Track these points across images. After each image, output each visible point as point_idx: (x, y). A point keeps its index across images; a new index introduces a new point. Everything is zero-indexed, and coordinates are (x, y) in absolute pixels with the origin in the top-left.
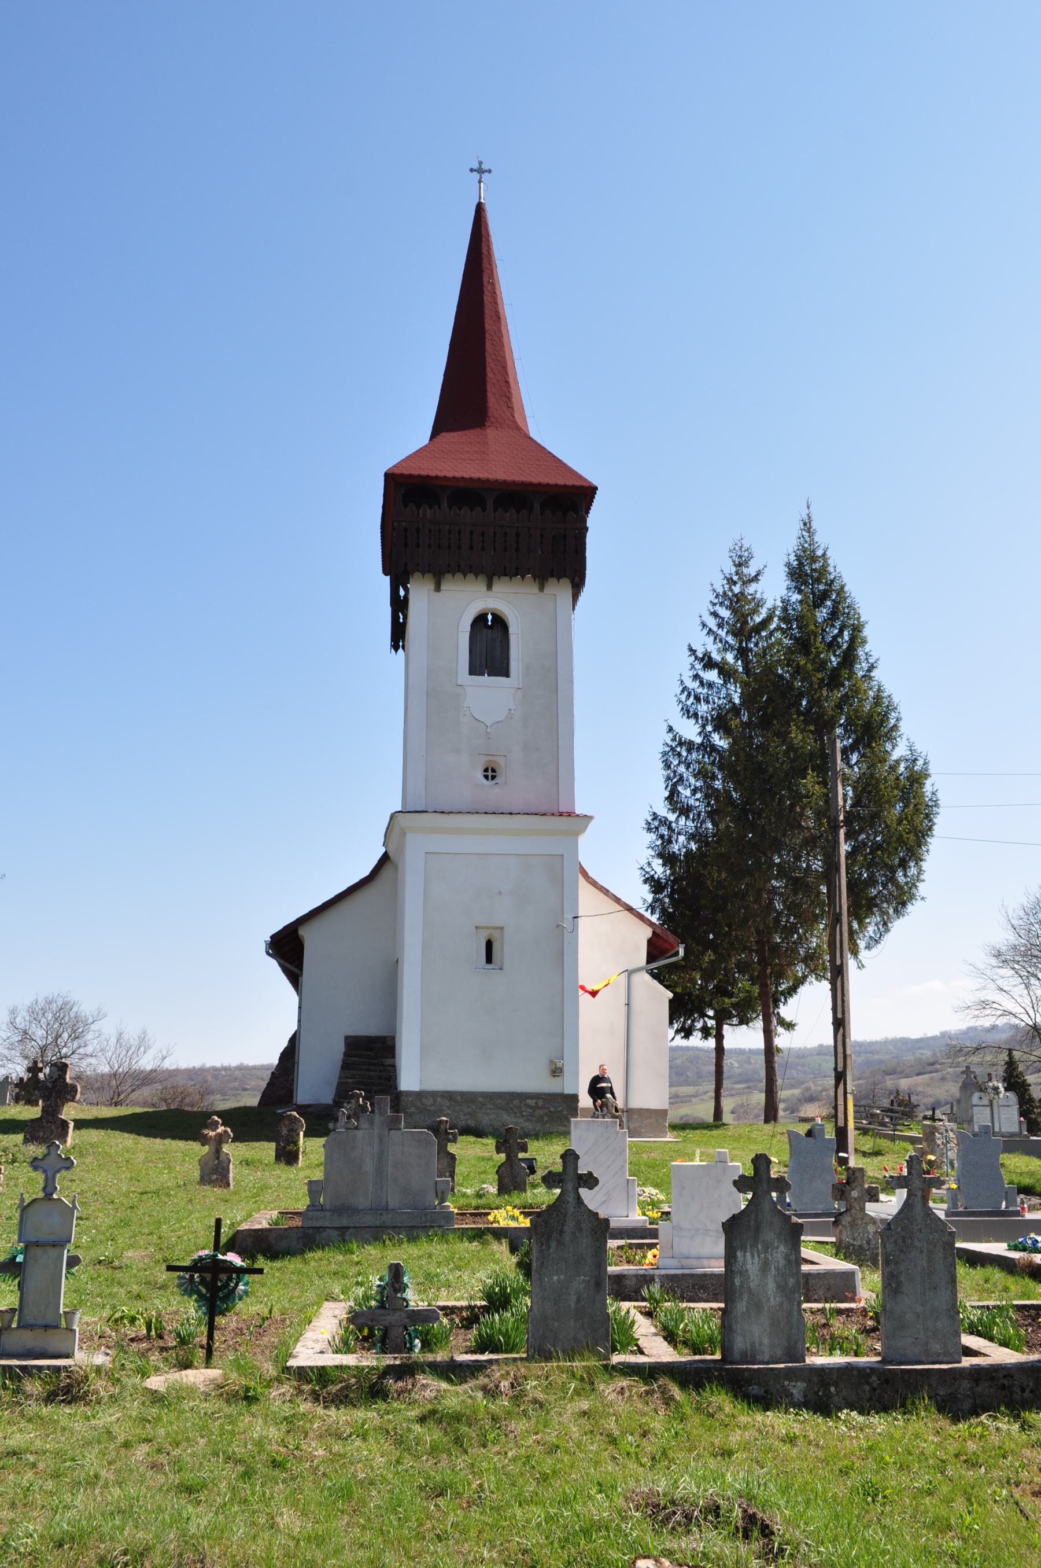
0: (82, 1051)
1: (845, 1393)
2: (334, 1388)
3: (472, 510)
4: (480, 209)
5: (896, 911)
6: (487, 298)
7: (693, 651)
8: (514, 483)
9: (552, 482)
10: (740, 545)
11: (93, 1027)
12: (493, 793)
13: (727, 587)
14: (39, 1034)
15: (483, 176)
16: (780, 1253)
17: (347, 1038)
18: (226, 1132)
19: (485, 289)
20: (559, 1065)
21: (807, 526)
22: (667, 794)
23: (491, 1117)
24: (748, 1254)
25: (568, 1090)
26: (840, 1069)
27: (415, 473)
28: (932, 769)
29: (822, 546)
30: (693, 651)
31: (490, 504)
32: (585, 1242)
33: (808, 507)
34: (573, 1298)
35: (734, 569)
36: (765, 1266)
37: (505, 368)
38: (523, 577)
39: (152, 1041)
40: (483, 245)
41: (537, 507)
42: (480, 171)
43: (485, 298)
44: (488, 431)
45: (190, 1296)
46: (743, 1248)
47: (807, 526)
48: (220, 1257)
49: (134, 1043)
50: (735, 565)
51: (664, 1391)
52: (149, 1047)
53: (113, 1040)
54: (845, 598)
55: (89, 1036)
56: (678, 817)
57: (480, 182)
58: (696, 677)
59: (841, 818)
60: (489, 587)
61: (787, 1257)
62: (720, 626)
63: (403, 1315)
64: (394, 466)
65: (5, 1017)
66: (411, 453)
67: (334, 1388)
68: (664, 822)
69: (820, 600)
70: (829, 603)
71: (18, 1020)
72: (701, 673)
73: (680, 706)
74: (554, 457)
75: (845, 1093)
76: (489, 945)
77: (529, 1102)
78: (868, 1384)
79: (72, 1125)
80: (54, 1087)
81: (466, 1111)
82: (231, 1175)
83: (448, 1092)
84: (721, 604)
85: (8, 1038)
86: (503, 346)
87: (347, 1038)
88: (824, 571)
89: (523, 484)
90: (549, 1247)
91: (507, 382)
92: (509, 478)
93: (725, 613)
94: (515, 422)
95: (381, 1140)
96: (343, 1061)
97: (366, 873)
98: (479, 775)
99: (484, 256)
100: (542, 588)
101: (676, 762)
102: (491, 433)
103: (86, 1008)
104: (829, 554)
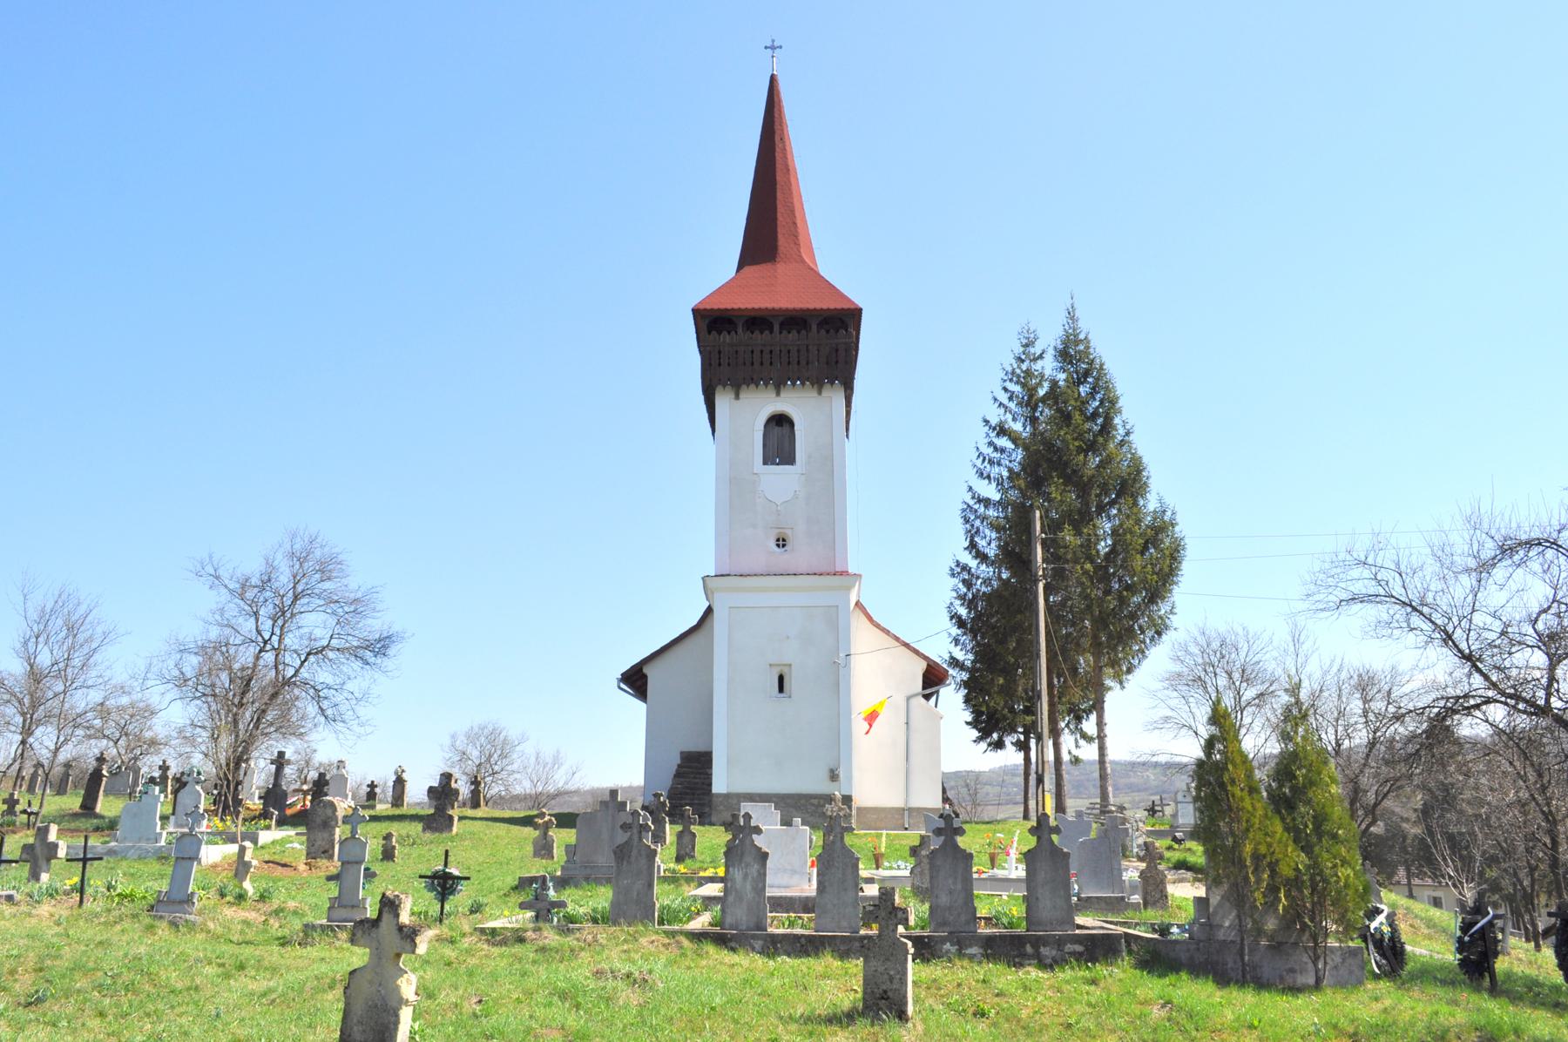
0: (509, 768)
2: (498, 938)
3: (762, 333)
4: (773, 79)
5: (1152, 639)
6: (778, 155)
8: (794, 310)
9: (825, 307)
11: (518, 748)
12: (782, 559)
13: (1015, 366)
14: (474, 753)
17: (682, 753)
18: (550, 820)
21: (1072, 316)
22: (967, 544)
27: (716, 307)
28: (1179, 518)
30: (986, 422)
31: (776, 328)
32: (643, 861)
35: (1022, 349)
36: (746, 876)
37: (793, 212)
40: (776, 110)
41: (814, 327)
42: (773, 48)
46: (733, 866)
47: (1072, 316)
48: (447, 870)
49: (550, 760)
50: (1023, 346)
51: (678, 942)
53: (533, 759)
54: (1105, 374)
55: (515, 756)
58: (991, 444)
59: (1041, 573)
60: (778, 394)
62: (1010, 399)
65: (447, 741)
66: (723, 282)
67: (498, 938)
68: (965, 568)
69: (1082, 378)
70: (1090, 380)
72: (996, 441)
73: (975, 470)
75: (1043, 791)
76: (781, 679)
77: (813, 801)
79: (456, 819)
80: (443, 791)
82: (555, 851)
83: (749, 794)
84: (1011, 380)
87: (682, 753)
88: (1086, 352)
91: (795, 223)
92: (790, 306)
93: (1017, 389)
94: (801, 256)
96: (677, 771)
97: (695, 623)
98: (772, 544)
100: (820, 393)
101: (972, 517)
103: (512, 733)
104: (1090, 337)
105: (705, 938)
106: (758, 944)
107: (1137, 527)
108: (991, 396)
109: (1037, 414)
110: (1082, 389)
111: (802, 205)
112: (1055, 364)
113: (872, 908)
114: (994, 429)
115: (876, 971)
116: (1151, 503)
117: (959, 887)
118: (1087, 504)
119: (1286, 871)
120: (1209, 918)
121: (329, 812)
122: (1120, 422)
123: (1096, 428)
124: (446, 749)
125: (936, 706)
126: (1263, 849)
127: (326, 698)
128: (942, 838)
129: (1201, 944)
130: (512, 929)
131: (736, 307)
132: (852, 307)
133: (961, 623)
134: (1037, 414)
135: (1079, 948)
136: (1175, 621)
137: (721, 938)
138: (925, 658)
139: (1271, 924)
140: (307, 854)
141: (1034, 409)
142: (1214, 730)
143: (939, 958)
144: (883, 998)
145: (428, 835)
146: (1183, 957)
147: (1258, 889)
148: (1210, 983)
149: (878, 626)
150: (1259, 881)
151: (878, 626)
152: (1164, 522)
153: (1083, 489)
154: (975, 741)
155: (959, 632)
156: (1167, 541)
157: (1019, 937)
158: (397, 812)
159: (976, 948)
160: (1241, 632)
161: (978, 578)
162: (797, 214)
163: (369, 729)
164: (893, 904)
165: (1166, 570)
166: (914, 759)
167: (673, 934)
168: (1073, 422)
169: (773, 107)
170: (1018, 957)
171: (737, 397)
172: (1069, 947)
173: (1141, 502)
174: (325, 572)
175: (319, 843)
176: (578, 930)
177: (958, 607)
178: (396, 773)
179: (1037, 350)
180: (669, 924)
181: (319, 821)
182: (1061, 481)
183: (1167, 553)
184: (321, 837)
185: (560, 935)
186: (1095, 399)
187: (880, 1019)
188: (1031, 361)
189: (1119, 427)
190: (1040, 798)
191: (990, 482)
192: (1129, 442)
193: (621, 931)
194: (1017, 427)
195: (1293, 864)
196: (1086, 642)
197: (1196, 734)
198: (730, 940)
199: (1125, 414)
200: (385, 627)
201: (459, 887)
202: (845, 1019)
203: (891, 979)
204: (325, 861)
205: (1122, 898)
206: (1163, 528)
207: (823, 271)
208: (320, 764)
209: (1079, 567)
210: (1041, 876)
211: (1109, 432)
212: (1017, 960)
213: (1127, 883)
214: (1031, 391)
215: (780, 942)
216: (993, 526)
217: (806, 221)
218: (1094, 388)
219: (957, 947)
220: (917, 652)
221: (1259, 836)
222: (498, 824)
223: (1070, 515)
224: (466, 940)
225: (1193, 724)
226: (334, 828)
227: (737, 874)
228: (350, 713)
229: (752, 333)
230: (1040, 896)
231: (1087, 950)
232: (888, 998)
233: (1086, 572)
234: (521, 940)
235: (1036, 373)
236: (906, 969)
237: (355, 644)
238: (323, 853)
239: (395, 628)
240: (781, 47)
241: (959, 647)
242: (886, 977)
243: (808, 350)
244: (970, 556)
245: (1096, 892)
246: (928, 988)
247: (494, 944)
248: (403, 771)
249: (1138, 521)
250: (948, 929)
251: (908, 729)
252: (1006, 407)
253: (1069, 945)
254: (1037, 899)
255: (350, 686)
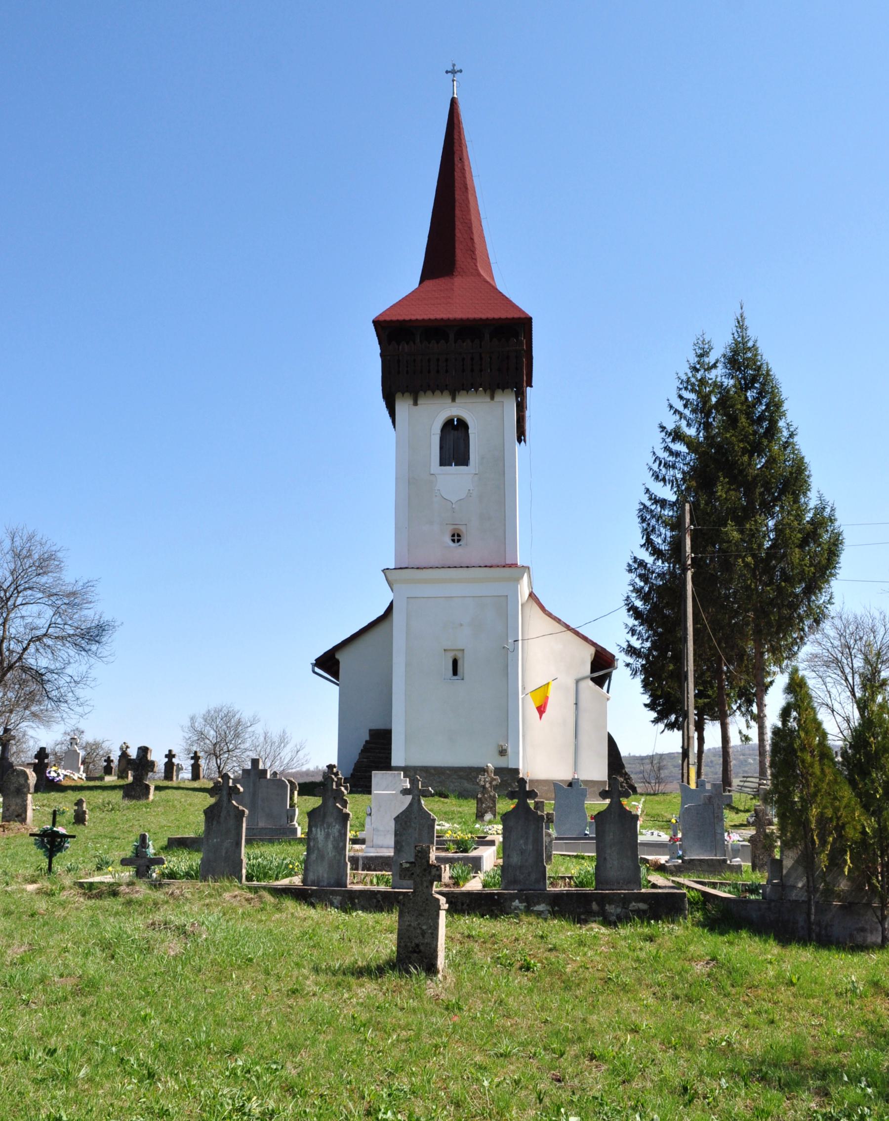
0: (242, 746)
1: (362, 903)
2: (94, 892)
3: (438, 343)
4: (453, 103)
5: (810, 627)
6: (457, 174)
7: (663, 428)
8: (468, 320)
9: (496, 316)
10: (701, 339)
11: (250, 729)
12: (457, 553)
13: (690, 375)
15: (456, 75)
16: (335, 830)
17: (370, 731)
19: (456, 167)
20: (504, 747)
21: (741, 325)
22: (643, 541)
23: (456, 784)
24: (319, 830)
25: (512, 766)
26: (686, 747)
27: (394, 318)
28: (837, 514)
29: (753, 339)
30: (663, 428)
31: (452, 337)
32: (232, 822)
33: (742, 308)
34: (224, 851)
35: (696, 359)
36: (327, 836)
37: (470, 228)
38: (476, 390)
39: (289, 738)
41: (487, 337)
42: (453, 72)
43: (456, 173)
44: (455, 279)
45: (41, 849)
47: (741, 325)
48: (55, 829)
49: (276, 739)
50: (699, 356)
51: (260, 897)
52: (287, 743)
53: (262, 739)
56: (655, 560)
57: (453, 81)
60: (454, 400)
61: (340, 831)
62: (685, 406)
63: (146, 860)
64: (380, 315)
65: (187, 723)
67: (94, 892)
68: (642, 564)
71: (196, 724)
72: (672, 445)
73: (651, 473)
74: (503, 296)
75: (688, 764)
76: (455, 663)
78: (376, 898)
81: (438, 780)
83: (425, 767)
84: (686, 389)
85: (190, 738)
86: (469, 211)
87: (370, 731)
88: (754, 360)
89: (475, 320)
90: (212, 825)
91: (472, 239)
93: (692, 396)
94: (477, 270)
95: (254, 784)
96: (364, 746)
97: (381, 612)
98: (448, 539)
99: (455, 141)
102: (458, 281)
103: (246, 715)
104: (758, 344)
105: (286, 894)
106: (337, 900)
107: (796, 523)
108: (667, 403)
109: (711, 420)
110: (749, 394)
111: (481, 222)
112: (724, 371)
113: (408, 865)
114: (670, 434)
115: (410, 925)
116: (812, 500)
117: (530, 847)
118: (751, 502)
119: (851, 833)
120: (781, 880)
121: (22, 781)
122: (785, 425)
123: (762, 431)
124: (186, 730)
125: (608, 692)
126: (829, 813)
127: (49, 681)
128: (516, 801)
129: (773, 904)
130: (108, 883)
131: (413, 318)
132: (522, 316)
133: (636, 613)
134: (711, 420)
135: (643, 906)
136: (832, 610)
137: (300, 895)
138: (594, 644)
139: (843, 885)
140: (3, 818)
141: (708, 415)
142: (791, 698)
143: (508, 914)
144: (415, 952)
145: (126, 802)
146: (754, 916)
147: (823, 851)
148: (771, 941)
149: (550, 615)
150: (824, 842)
151: (550, 615)
152: (824, 518)
153: (749, 487)
154: (653, 722)
155: (636, 623)
156: (826, 537)
157: (586, 895)
158: (196, 784)
159: (543, 905)
160: (877, 614)
161: (653, 572)
162: (475, 231)
163: (87, 709)
164: (428, 861)
165: (824, 562)
166: (583, 738)
167: (255, 890)
168: (739, 424)
169: (454, 128)
170: (583, 914)
171: (416, 403)
172: (634, 905)
173: (802, 500)
174: (44, 565)
175: (13, 807)
176: (168, 884)
177: (633, 599)
178: (121, 749)
179: (711, 359)
180: (258, 881)
181: (12, 788)
182: (727, 480)
183: (826, 547)
184: (14, 802)
185: (150, 889)
186: (761, 404)
187: (408, 972)
188: (705, 370)
189: (784, 429)
190: (685, 771)
191: (665, 484)
192: (794, 444)
193: (206, 887)
194: (691, 432)
195: (859, 827)
196: (749, 630)
197: (833, 711)
198: (311, 896)
199: (790, 416)
200: (97, 617)
201: (66, 845)
202: (375, 972)
203: (423, 934)
204: (18, 824)
205: (725, 861)
206: (822, 524)
207: (501, 287)
208: (87, 743)
209: (740, 560)
210: (610, 837)
211: (774, 434)
212: (583, 917)
213: (730, 846)
214: (705, 399)
215: (358, 898)
216: (665, 524)
217: (484, 237)
218: (760, 393)
219: (525, 904)
220: (585, 639)
221: (827, 801)
222: (197, 793)
223: (734, 512)
224: (65, 893)
225: (830, 703)
226: (26, 795)
227: (320, 834)
228: (71, 694)
229: (429, 343)
230: (608, 857)
231: (650, 908)
232: (420, 952)
233: (747, 565)
234: (115, 894)
235: (710, 382)
236: (437, 924)
237: (71, 632)
238: (17, 816)
239: (106, 617)
240: (461, 71)
241: (635, 637)
242: (419, 931)
243: (481, 359)
244: (647, 554)
245: (698, 855)
246: (484, 942)
247: (90, 898)
248: (127, 747)
249: (799, 517)
250: (519, 887)
251: (577, 709)
252: (681, 414)
253: (634, 904)
254: (605, 859)
255: (69, 671)
